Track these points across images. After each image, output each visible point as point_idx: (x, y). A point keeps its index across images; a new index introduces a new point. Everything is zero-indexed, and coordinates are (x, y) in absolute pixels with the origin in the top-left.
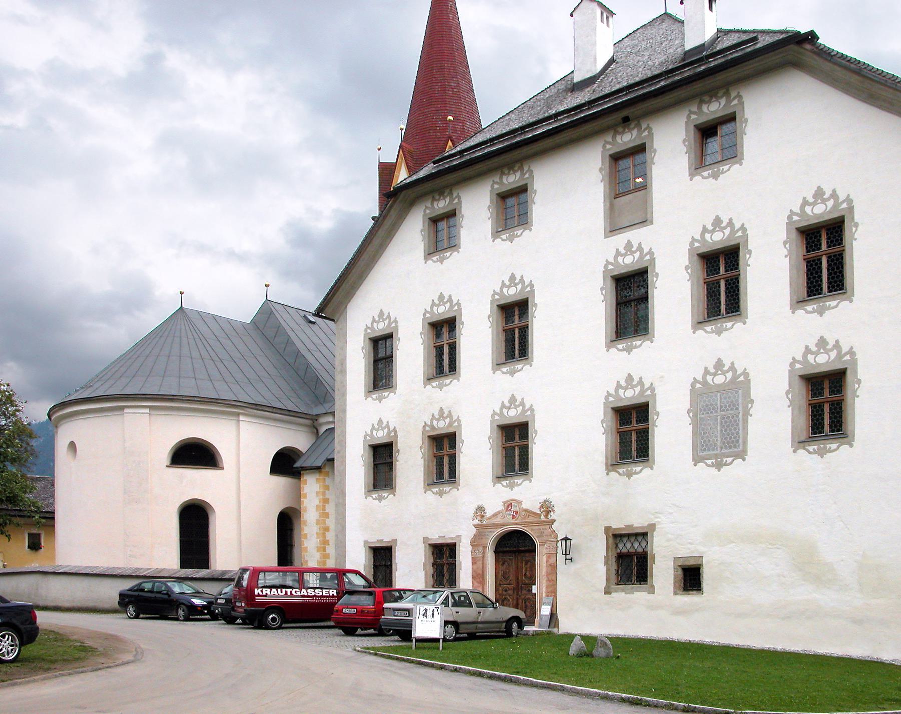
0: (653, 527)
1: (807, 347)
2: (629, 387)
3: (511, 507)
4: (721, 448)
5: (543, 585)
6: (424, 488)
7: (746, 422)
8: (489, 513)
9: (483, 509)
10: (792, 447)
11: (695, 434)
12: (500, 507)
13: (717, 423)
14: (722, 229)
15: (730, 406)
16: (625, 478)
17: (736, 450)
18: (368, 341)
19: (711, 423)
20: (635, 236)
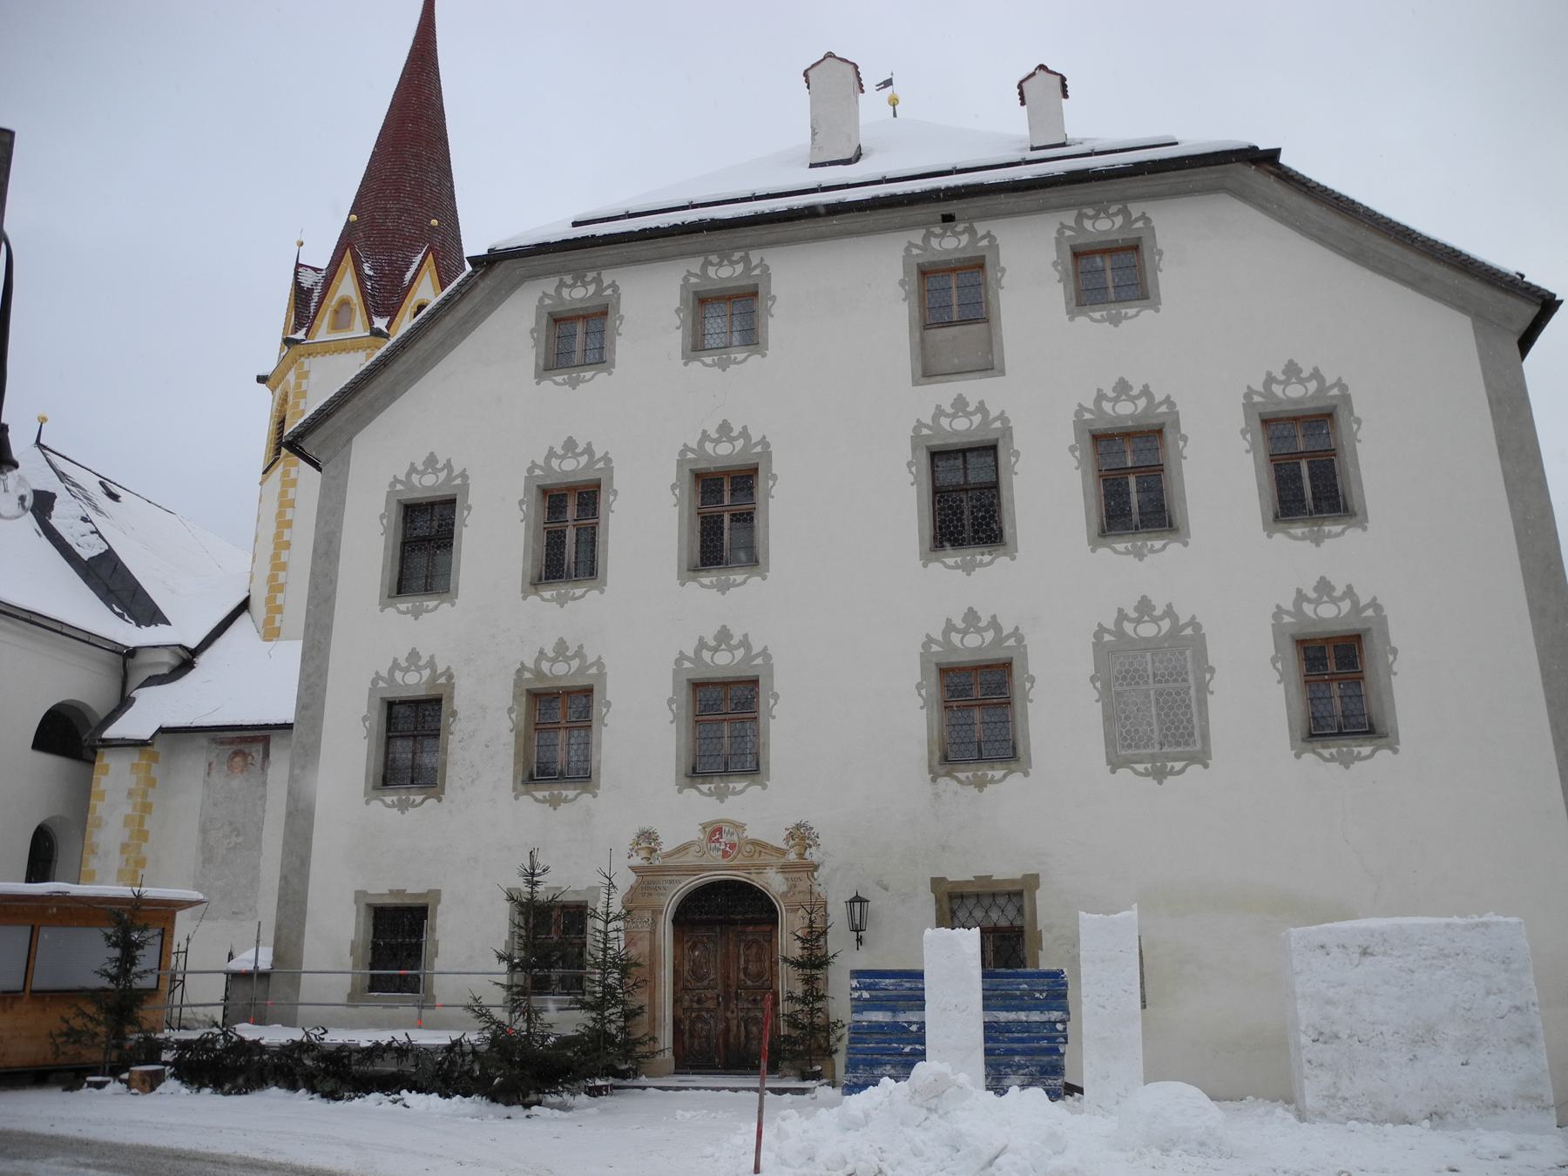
1: (701, 639)
4: (1162, 745)
6: (514, 789)
7: (1203, 703)
8: (667, 844)
9: (653, 836)
10: (1292, 749)
11: (1108, 719)
12: (694, 833)
13: (1150, 702)
14: (436, 471)
15: (1171, 675)
17: (1188, 749)
18: (394, 506)
19: (1139, 701)
20: (974, 389)
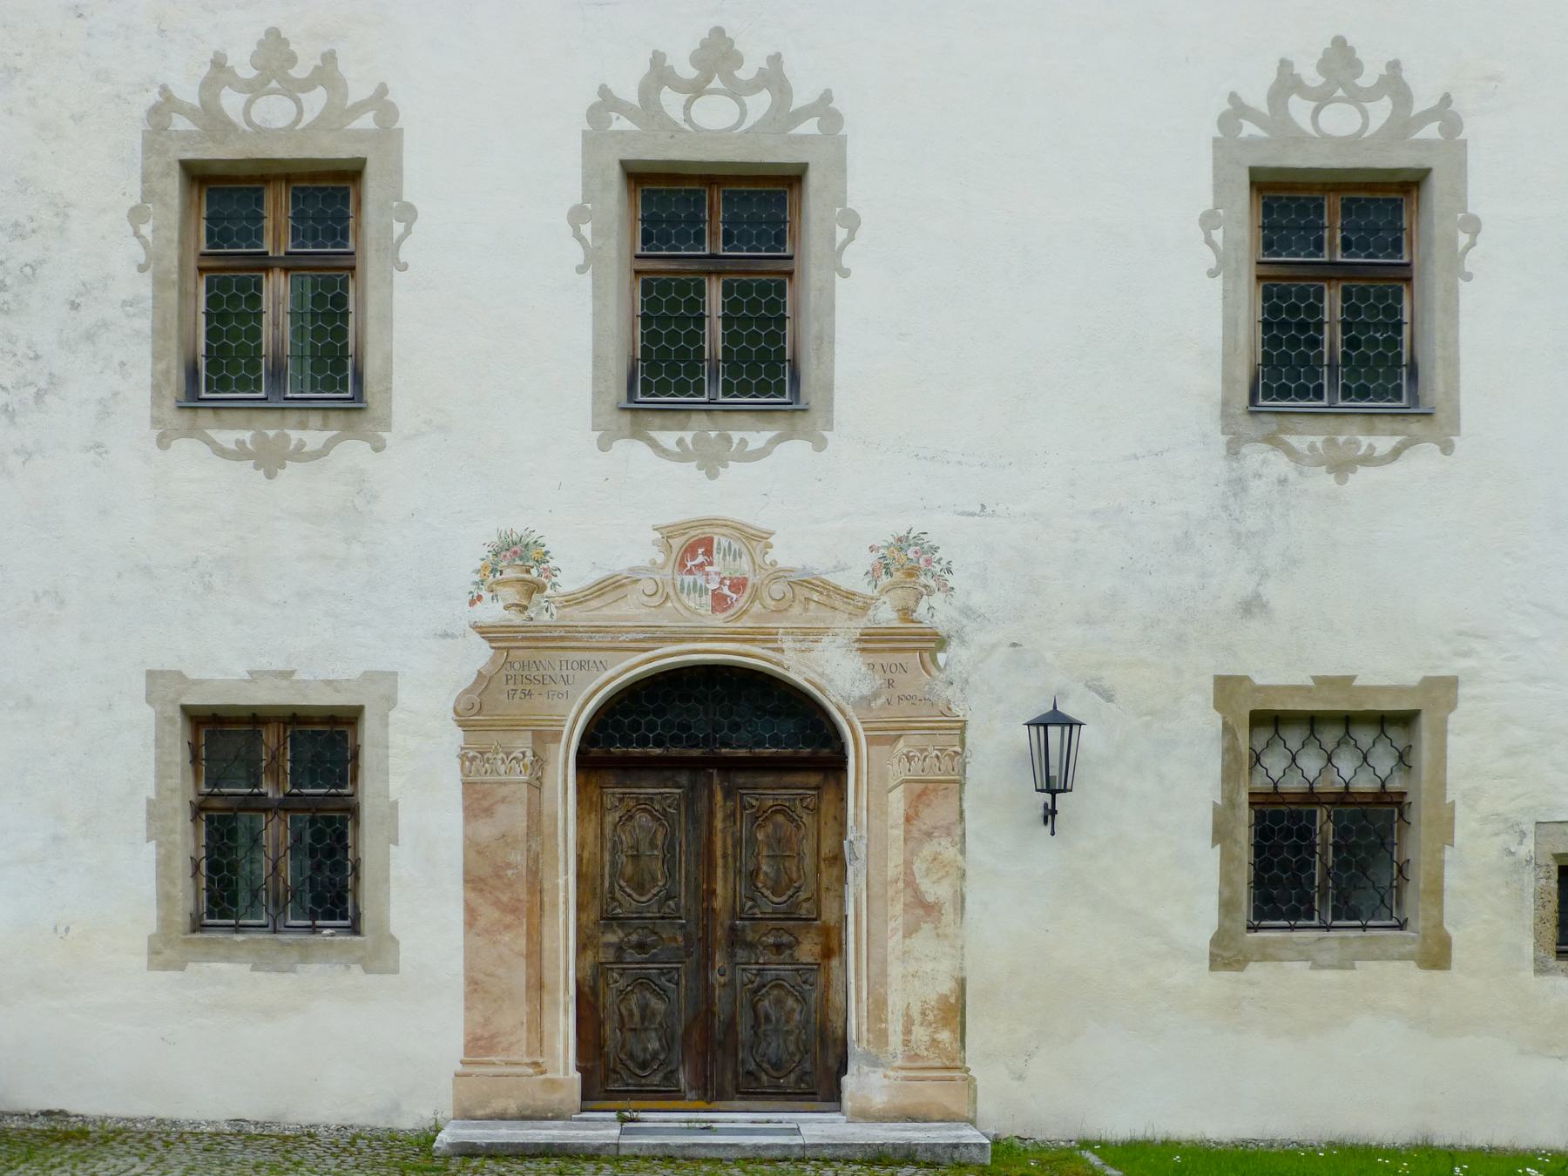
0: (1444, 689)
2: (1340, 92)
3: (708, 553)
5: (892, 925)
6: (156, 421)
16: (1323, 480)
